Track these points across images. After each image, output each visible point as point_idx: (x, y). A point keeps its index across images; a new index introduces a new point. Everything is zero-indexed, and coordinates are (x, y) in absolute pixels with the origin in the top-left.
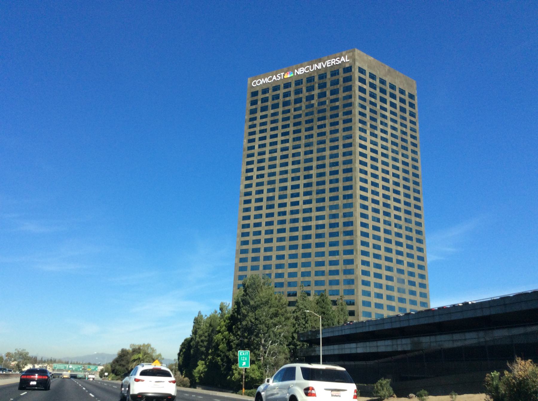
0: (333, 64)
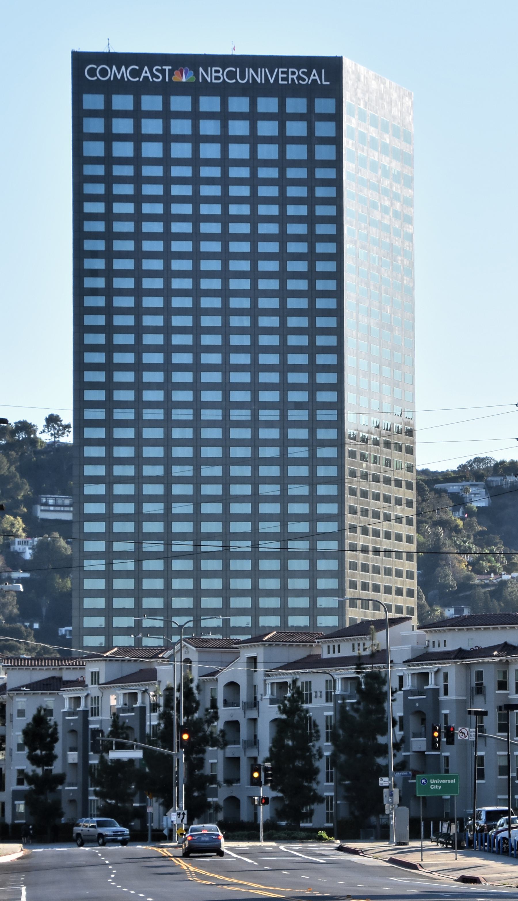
0: (293, 79)
